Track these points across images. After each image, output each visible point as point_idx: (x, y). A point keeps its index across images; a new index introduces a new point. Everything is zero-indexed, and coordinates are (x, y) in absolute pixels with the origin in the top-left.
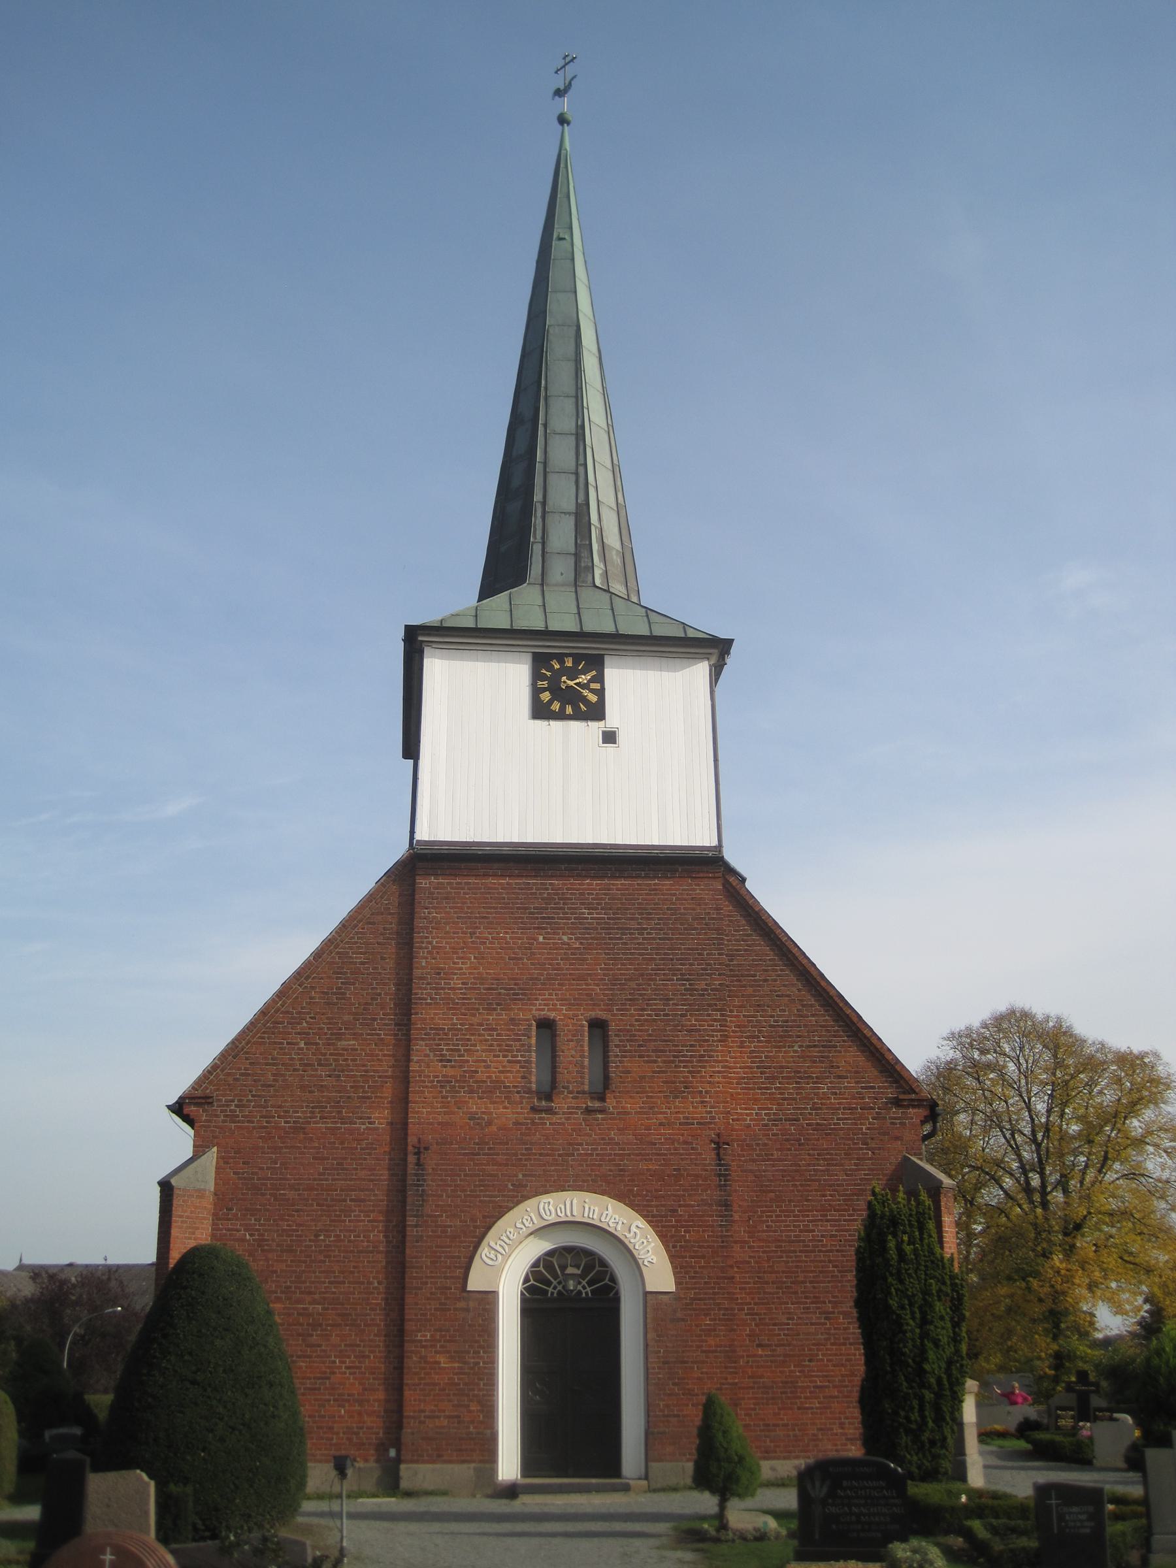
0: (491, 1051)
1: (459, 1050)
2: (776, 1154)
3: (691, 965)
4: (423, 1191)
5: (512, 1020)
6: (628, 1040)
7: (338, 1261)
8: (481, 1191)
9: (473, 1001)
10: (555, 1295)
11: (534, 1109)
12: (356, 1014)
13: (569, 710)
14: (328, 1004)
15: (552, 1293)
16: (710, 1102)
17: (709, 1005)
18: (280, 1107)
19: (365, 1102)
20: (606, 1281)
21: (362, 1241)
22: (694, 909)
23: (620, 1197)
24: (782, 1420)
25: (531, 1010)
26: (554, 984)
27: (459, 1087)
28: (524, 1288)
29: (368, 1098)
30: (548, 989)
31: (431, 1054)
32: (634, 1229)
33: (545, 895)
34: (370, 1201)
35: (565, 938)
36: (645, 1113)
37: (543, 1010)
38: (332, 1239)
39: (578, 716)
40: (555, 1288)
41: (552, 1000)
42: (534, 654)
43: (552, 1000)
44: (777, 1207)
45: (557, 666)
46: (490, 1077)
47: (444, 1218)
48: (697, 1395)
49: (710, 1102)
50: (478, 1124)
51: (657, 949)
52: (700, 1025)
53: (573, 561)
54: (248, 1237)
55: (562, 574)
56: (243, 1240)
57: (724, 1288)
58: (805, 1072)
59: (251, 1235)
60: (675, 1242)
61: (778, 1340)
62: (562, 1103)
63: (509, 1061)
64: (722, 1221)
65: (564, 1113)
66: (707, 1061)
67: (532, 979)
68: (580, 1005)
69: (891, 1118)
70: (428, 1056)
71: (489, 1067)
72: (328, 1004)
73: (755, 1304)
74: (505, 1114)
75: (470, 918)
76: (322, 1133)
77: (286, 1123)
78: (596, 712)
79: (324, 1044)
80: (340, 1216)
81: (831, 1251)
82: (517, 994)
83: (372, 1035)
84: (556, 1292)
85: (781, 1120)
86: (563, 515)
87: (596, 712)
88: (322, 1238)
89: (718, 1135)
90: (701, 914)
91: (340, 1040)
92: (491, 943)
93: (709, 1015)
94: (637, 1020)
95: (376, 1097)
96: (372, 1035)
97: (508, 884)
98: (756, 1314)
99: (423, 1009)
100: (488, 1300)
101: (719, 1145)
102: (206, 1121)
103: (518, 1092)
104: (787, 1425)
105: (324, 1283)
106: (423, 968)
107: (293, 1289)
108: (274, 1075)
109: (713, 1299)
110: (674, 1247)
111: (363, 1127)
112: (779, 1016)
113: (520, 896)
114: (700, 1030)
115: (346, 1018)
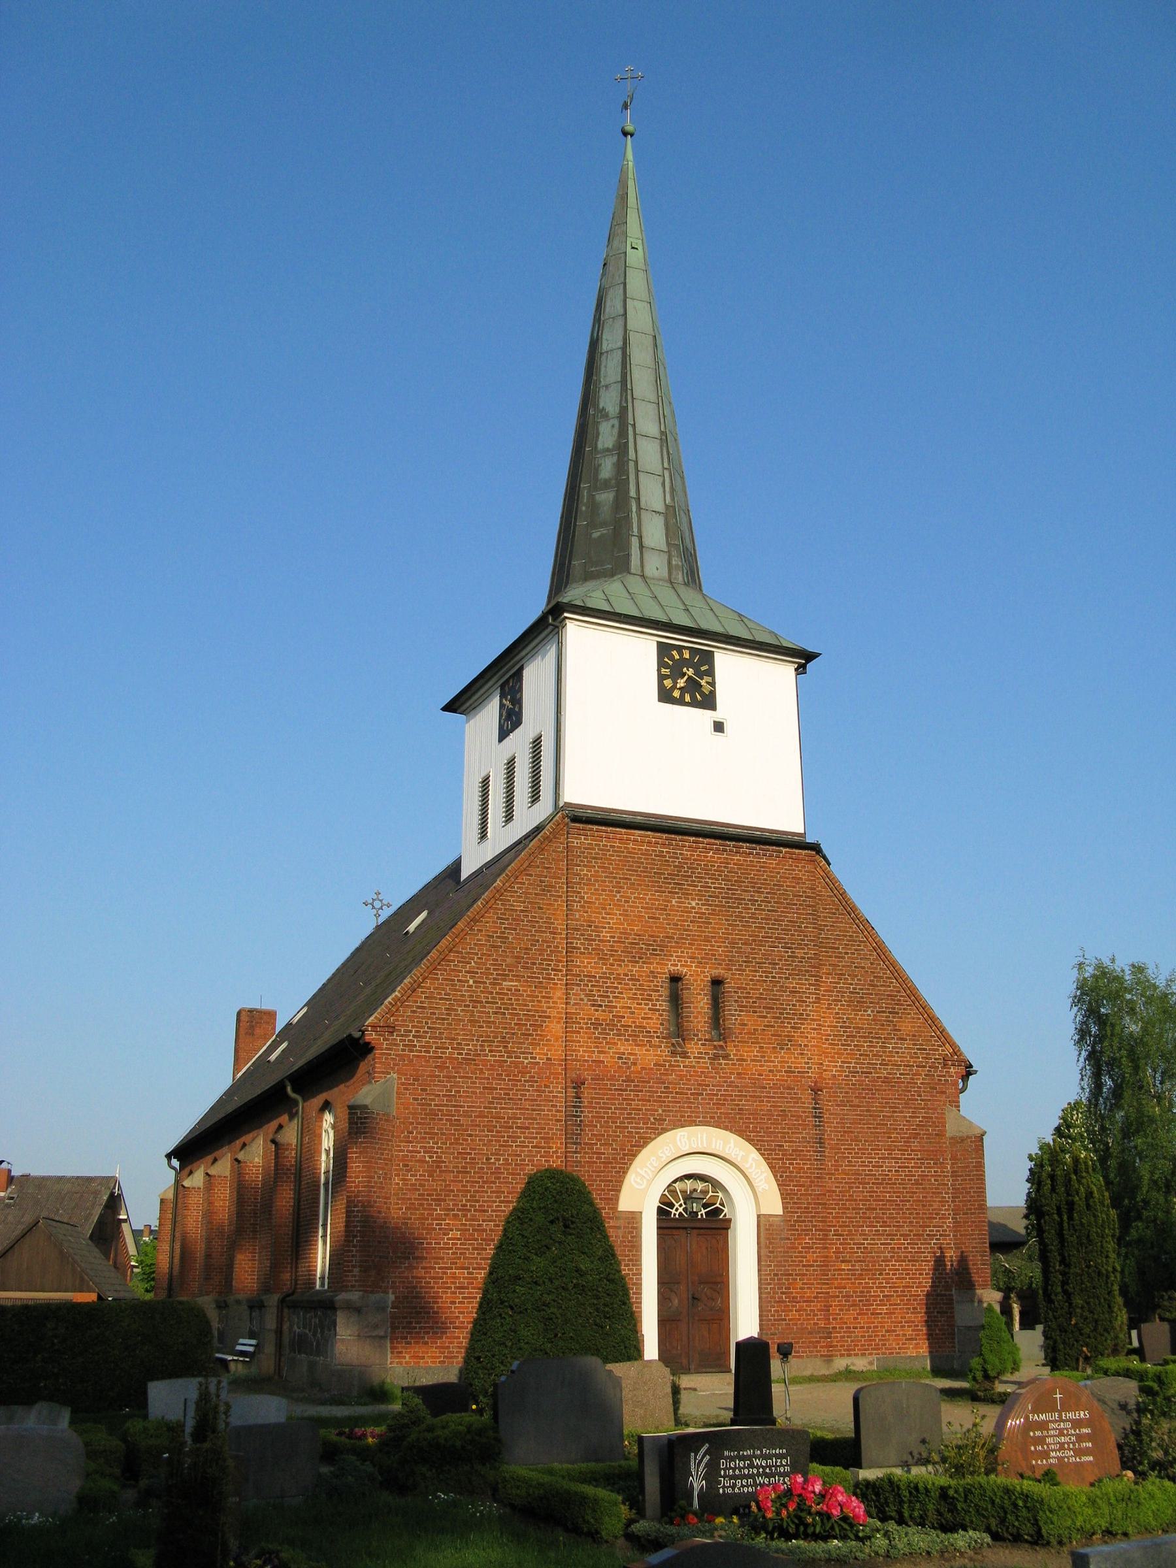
0: (634, 999)
1: (608, 997)
2: (856, 1101)
3: (792, 935)
4: (581, 1121)
5: (652, 972)
6: (744, 998)
7: (506, 1183)
8: (629, 1123)
9: (619, 953)
10: (677, 1216)
11: (674, 1053)
12: (518, 957)
13: (687, 698)
14: (493, 946)
15: (675, 1215)
16: (808, 1054)
17: (807, 971)
18: (454, 1039)
19: (528, 1039)
20: (718, 1205)
21: (528, 1165)
22: (794, 887)
23: (740, 1133)
24: (860, 1323)
25: (667, 965)
26: (685, 943)
27: (610, 1030)
28: (723, 1211)
29: (530, 1035)
30: (680, 948)
31: (586, 999)
32: (750, 1159)
33: (677, 864)
34: (533, 1128)
35: (694, 904)
36: (758, 1061)
37: (677, 965)
38: (501, 1162)
39: (694, 704)
40: (677, 1210)
41: (684, 957)
42: (658, 643)
43: (684, 957)
44: (856, 1145)
45: (677, 657)
46: (634, 1022)
47: (599, 1146)
48: (799, 1302)
49: (808, 1054)
50: (625, 1063)
51: (767, 919)
52: (799, 988)
53: (667, 557)
54: (427, 1159)
55: (657, 569)
56: (423, 1161)
57: (818, 1213)
58: (876, 1033)
59: (431, 1157)
60: (783, 1172)
61: (857, 1257)
62: (694, 1048)
63: (650, 1009)
64: (817, 1156)
65: (695, 1057)
66: (805, 1019)
67: (667, 937)
68: (707, 963)
69: (938, 1076)
70: (582, 1000)
71: (633, 1013)
72: (493, 946)
73: (840, 1226)
74: (649, 1055)
75: (615, 878)
76: (491, 1065)
77: (458, 1054)
78: (708, 702)
79: (490, 984)
80: (508, 1141)
81: (895, 1184)
82: (656, 950)
83: (532, 977)
84: (677, 1213)
85: (858, 1072)
86: (654, 513)
87: (708, 702)
88: (492, 1161)
89: (816, 1083)
90: (799, 892)
91: (505, 980)
92: (633, 902)
93: (806, 980)
94: (751, 980)
95: (537, 1035)
96: (532, 977)
97: (646, 850)
98: (841, 1235)
99: (577, 957)
100: (634, 1219)
101: (816, 1090)
102: (387, 1049)
103: (658, 1037)
104: (863, 1327)
105: (495, 1202)
106: (577, 920)
107: (468, 1207)
108: (447, 1009)
109: (811, 1222)
110: (781, 1176)
111: (526, 1061)
112: (856, 984)
113: (656, 862)
114: (799, 992)
115: (509, 960)
